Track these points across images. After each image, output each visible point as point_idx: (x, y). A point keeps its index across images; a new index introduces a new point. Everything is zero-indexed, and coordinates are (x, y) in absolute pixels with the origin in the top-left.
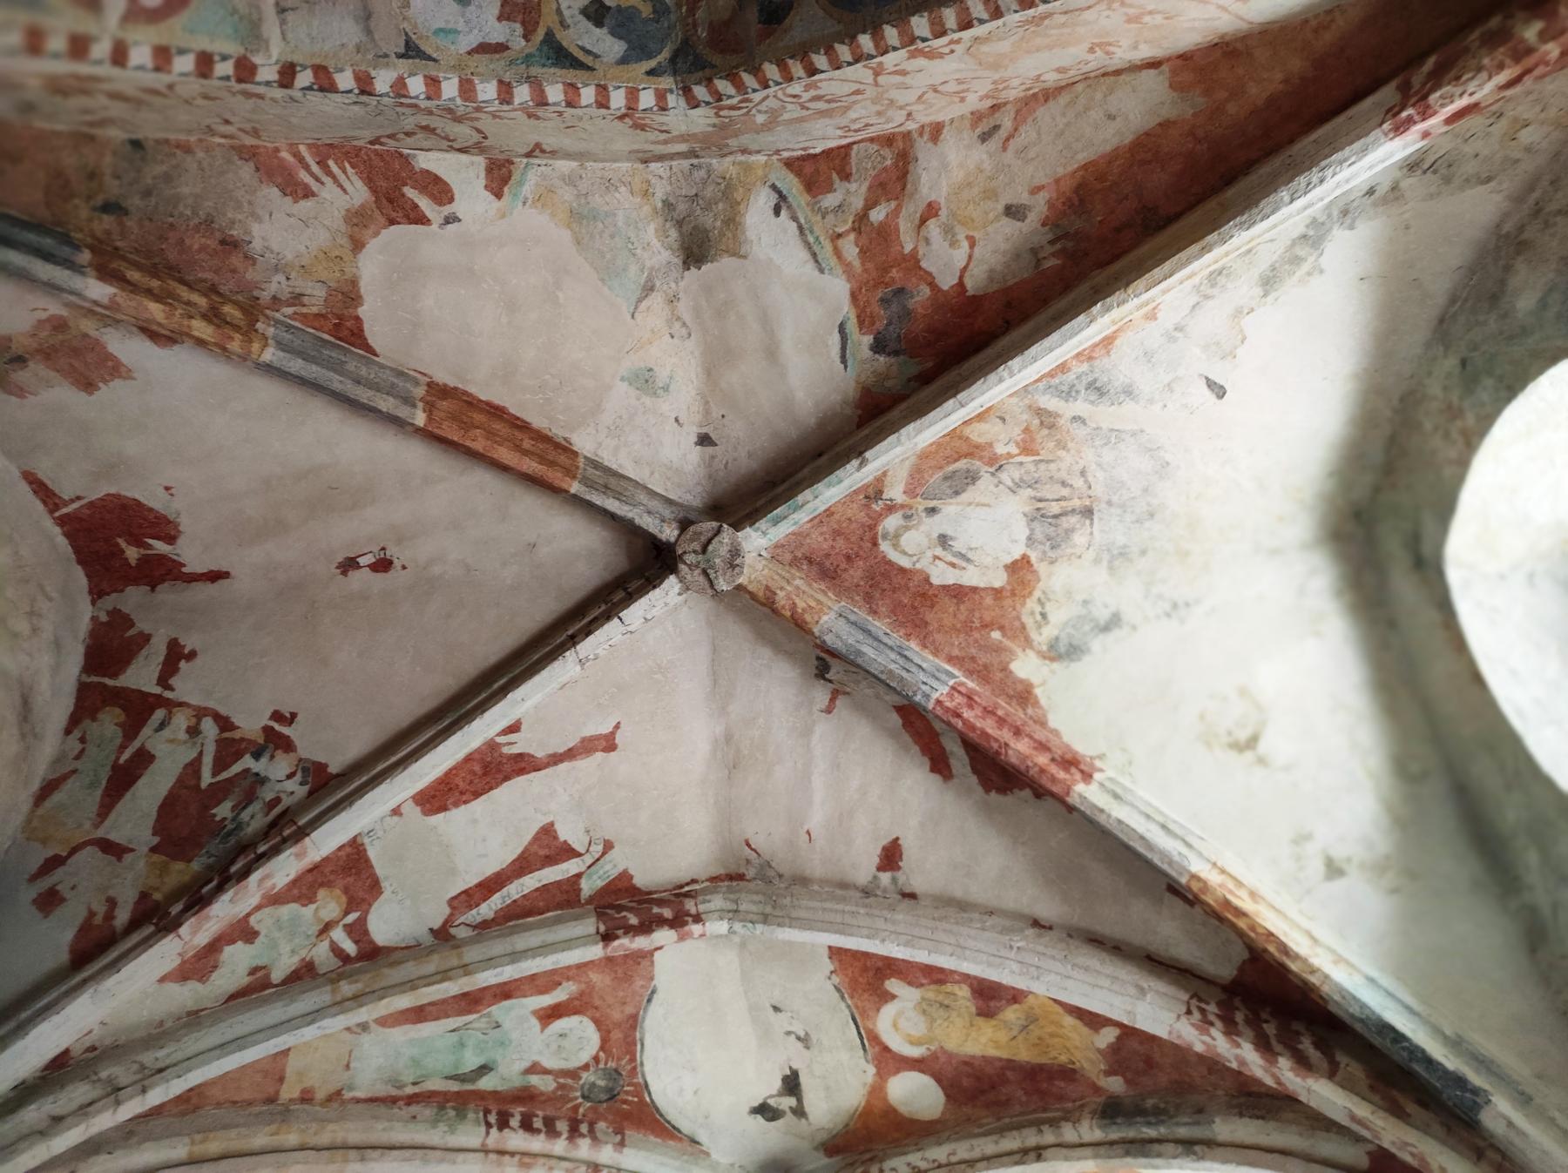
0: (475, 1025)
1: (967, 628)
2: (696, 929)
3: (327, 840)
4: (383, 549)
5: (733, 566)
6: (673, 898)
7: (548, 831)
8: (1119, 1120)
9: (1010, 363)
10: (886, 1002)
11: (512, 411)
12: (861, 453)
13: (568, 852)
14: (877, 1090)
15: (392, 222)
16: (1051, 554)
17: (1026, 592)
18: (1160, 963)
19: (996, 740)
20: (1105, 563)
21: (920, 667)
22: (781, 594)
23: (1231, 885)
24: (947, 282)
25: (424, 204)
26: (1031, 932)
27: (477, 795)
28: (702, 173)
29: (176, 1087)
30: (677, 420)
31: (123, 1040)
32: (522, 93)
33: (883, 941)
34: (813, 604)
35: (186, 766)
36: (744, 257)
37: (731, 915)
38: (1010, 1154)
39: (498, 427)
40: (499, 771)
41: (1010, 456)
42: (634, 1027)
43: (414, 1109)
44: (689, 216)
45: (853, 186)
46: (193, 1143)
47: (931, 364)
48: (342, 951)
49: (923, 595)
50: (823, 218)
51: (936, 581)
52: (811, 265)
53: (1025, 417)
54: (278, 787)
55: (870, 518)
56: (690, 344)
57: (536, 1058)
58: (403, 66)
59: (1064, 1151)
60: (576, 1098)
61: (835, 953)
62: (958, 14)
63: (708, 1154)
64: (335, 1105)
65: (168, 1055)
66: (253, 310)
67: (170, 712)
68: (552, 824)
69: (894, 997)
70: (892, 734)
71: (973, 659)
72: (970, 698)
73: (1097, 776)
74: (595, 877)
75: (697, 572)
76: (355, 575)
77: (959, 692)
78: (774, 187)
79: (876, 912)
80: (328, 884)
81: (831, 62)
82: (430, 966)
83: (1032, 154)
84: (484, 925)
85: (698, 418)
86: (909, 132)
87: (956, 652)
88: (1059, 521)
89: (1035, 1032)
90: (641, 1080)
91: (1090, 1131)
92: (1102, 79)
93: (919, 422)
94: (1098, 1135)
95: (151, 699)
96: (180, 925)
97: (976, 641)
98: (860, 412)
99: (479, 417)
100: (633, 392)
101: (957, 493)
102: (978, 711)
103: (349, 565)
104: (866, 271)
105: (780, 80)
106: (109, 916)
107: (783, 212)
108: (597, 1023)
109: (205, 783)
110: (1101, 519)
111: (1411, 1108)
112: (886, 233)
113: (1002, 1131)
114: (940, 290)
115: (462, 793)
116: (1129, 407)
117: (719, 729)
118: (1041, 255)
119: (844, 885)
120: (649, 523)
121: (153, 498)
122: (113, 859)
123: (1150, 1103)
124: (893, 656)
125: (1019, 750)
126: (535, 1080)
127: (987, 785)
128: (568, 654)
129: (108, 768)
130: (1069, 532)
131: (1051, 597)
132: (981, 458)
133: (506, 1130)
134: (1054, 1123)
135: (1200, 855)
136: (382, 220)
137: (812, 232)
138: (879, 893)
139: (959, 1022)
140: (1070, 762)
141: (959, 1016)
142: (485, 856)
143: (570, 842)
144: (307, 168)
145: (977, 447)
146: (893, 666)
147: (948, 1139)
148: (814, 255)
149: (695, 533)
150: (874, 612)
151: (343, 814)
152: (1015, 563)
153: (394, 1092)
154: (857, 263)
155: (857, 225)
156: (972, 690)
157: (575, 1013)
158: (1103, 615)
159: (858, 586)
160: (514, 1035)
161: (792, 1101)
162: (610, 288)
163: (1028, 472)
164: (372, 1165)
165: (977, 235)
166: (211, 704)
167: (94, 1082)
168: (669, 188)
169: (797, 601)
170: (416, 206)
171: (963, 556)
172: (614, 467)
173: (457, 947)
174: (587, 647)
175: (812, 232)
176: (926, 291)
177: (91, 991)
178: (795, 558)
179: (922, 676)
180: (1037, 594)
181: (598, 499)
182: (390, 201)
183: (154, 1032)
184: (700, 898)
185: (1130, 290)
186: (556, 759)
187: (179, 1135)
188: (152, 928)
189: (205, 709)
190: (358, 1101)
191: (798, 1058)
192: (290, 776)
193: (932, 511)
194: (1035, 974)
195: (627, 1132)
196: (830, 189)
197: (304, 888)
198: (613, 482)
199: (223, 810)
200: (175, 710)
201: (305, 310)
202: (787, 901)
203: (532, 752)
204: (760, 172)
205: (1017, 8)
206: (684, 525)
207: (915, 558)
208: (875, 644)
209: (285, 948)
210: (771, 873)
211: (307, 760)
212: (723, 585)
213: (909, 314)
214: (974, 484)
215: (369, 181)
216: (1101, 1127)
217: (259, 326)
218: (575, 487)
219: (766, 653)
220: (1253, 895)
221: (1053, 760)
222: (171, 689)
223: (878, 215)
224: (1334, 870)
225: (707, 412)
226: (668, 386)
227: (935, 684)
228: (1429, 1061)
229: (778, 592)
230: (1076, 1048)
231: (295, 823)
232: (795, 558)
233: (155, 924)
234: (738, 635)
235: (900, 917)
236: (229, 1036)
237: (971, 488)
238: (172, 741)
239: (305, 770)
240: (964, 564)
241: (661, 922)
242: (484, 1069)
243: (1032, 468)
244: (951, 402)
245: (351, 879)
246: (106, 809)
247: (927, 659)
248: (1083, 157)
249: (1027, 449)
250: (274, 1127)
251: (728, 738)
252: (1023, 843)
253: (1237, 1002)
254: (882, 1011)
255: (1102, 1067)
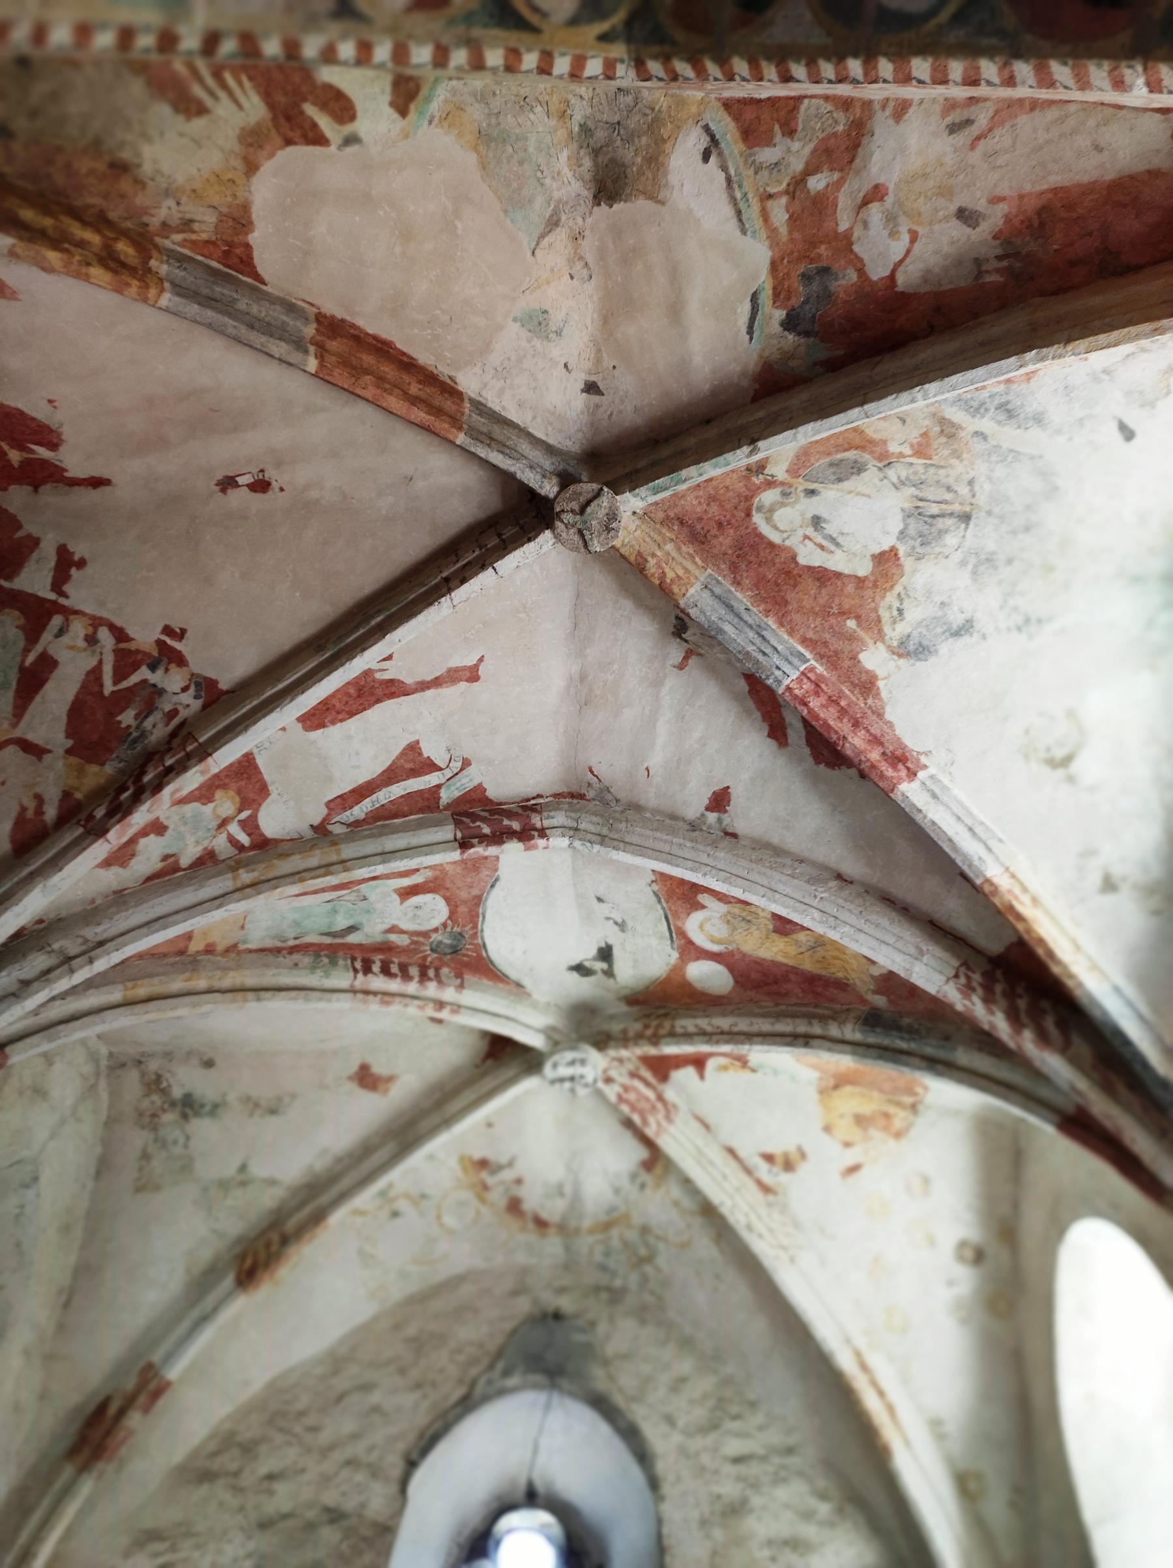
0: (345, 898)
1: (825, 613)
2: (541, 842)
3: (226, 756)
4: (262, 471)
5: (608, 529)
6: (520, 811)
7: (413, 748)
8: (878, 1030)
9: (927, 386)
10: (697, 910)
11: (399, 346)
12: (753, 441)
13: (431, 767)
14: (678, 969)
15: (289, 142)
16: (919, 550)
17: (888, 585)
18: (941, 929)
19: (836, 732)
20: (970, 567)
21: (776, 649)
22: (652, 562)
23: (1017, 890)
24: (877, 272)
25: (324, 123)
26: (833, 884)
27: (351, 714)
28: (629, 99)
29: (116, 957)
30: (566, 366)
31: (64, 914)
32: (459, 57)
33: (705, 875)
34: (681, 572)
35: (88, 673)
36: (663, 203)
37: (572, 833)
38: (782, 1035)
39: (387, 369)
40: (372, 694)
41: (901, 455)
42: (478, 905)
43: (296, 957)
44: (607, 145)
45: (796, 146)
46: (126, 989)
47: (842, 352)
48: (238, 841)
49: (788, 573)
50: (756, 173)
51: (802, 560)
52: (734, 222)
53: (927, 422)
54: (175, 699)
55: (748, 489)
56: (590, 287)
57: (395, 922)
58: (333, 29)
59: (829, 1044)
60: (426, 951)
61: (662, 877)
62: (965, 70)
63: (529, 995)
64: (233, 955)
65: (105, 930)
66: (143, 241)
67: (67, 620)
68: (418, 742)
69: (703, 907)
70: (736, 697)
71: (825, 644)
72: (817, 685)
73: (921, 775)
74: (453, 788)
75: (572, 531)
76: (233, 494)
77: (808, 678)
78: (707, 129)
79: (701, 847)
80: (224, 787)
81: (810, 75)
82: (314, 859)
83: (1001, 161)
84: (357, 824)
85: (588, 365)
86: (870, 102)
87: (810, 635)
88: (935, 521)
89: (821, 952)
90: (480, 941)
91: (851, 1032)
92: (1100, 108)
93: (819, 423)
94: (858, 1036)
95: (47, 605)
96: (107, 831)
97: (831, 627)
98: (757, 386)
99: (368, 359)
100: (524, 334)
101: (840, 480)
102: (823, 699)
103: (228, 483)
104: (792, 240)
105: (748, 77)
106: (39, 812)
107: (713, 159)
108: (448, 900)
109: (107, 692)
110: (976, 525)
111: (1121, 1089)
112: (821, 205)
113: (778, 1016)
114: (868, 279)
115: (338, 713)
116: (1035, 433)
117: (575, 668)
118: (984, 268)
119: (674, 817)
120: (530, 478)
121: (37, 409)
122: (34, 758)
123: (906, 1021)
124: (751, 634)
125: (855, 742)
126: (393, 937)
127: (818, 758)
128: (443, 599)
129: (16, 670)
130: (942, 533)
131: (911, 594)
132: (871, 453)
133: (370, 975)
134: (823, 1019)
135: (997, 858)
136: (279, 140)
137: (740, 186)
138: (704, 828)
139: (756, 934)
140: (900, 758)
141: (758, 929)
142: (358, 767)
143: (433, 759)
144: (200, 80)
145: (871, 441)
146: (750, 648)
147: (732, 1013)
148: (739, 213)
149: (575, 493)
150: (737, 583)
151: (240, 738)
152: (882, 554)
153: (279, 944)
154: (784, 231)
155: (791, 188)
156: (821, 676)
157: (429, 892)
158: (956, 619)
159: (725, 554)
160: (378, 906)
161: (604, 966)
162: (512, 221)
163: (915, 473)
164: (264, 1003)
165: (921, 231)
166: (104, 614)
167: (49, 953)
168: (589, 111)
169: (667, 570)
170: (314, 126)
171: (833, 540)
172: (497, 408)
173: (334, 843)
174: (462, 593)
175: (740, 186)
176: (852, 276)
177: (41, 886)
178: (668, 517)
179: (776, 660)
180: (898, 588)
181: (482, 452)
182: (289, 118)
183: (89, 907)
184: (545, 814)
185: (1070, 347)
186: (423, 686)
187: (113, 983)
188: (81, 830)
189: (101, 618)
190: (250, 951)
191: (613, 936)
192: (185, 689)
193: (811, 493)
194: (833, 924)
195: (466, 977)
196: (769, 142)
197: (204, 794)
198: (497, 431)
199: (127, 718)
200: (72, 617)
201: (194, 237)
202: (623, 826)
203: (402, 679)
204: (694, 109)
205: (1034, 84)
206: (566, 480)
207: (785, 535)
208: (736, 620)
209: (190, 840)
210: (609, 797)
211: (199, 676)
212: (596, 546)
213: (829, 296)
214: (859, 474)
215: (267, 96)
216: (862, 1032)
217: (153, 263)
218: (461, 439)
219: (628, 605)
220: (1035, 901)
221: (884, 754)
222: (67, 597)
223: (817, 183)
224: (1109, 885)
225: (598, 361)
226: (561, 330)
227: (786, 668)
228: (1145, 1065)
229: (649, 559)
230: (853, 970)
231: (196, 740)
232: (668, 517)
233: (84, 826)
234: (602, 583)
235: (722, 855)
236: (152, 915)
237: (854, 477)
238: (72, 648)
239: (197, 684)
240: (833, 548)
241: (511, 834)
242: (352, 929)
243: (921, 470)
244: (857, 410)
245: (243, 783)
246: (19, 710)
247: (782, 639)
248: (1056, 180)
249: (921, 451)
250: (187, 975)
251: (583, 678)
252: (840, 812)
253: (999, 974)
254: (692, 915)
255: (872, 987)
